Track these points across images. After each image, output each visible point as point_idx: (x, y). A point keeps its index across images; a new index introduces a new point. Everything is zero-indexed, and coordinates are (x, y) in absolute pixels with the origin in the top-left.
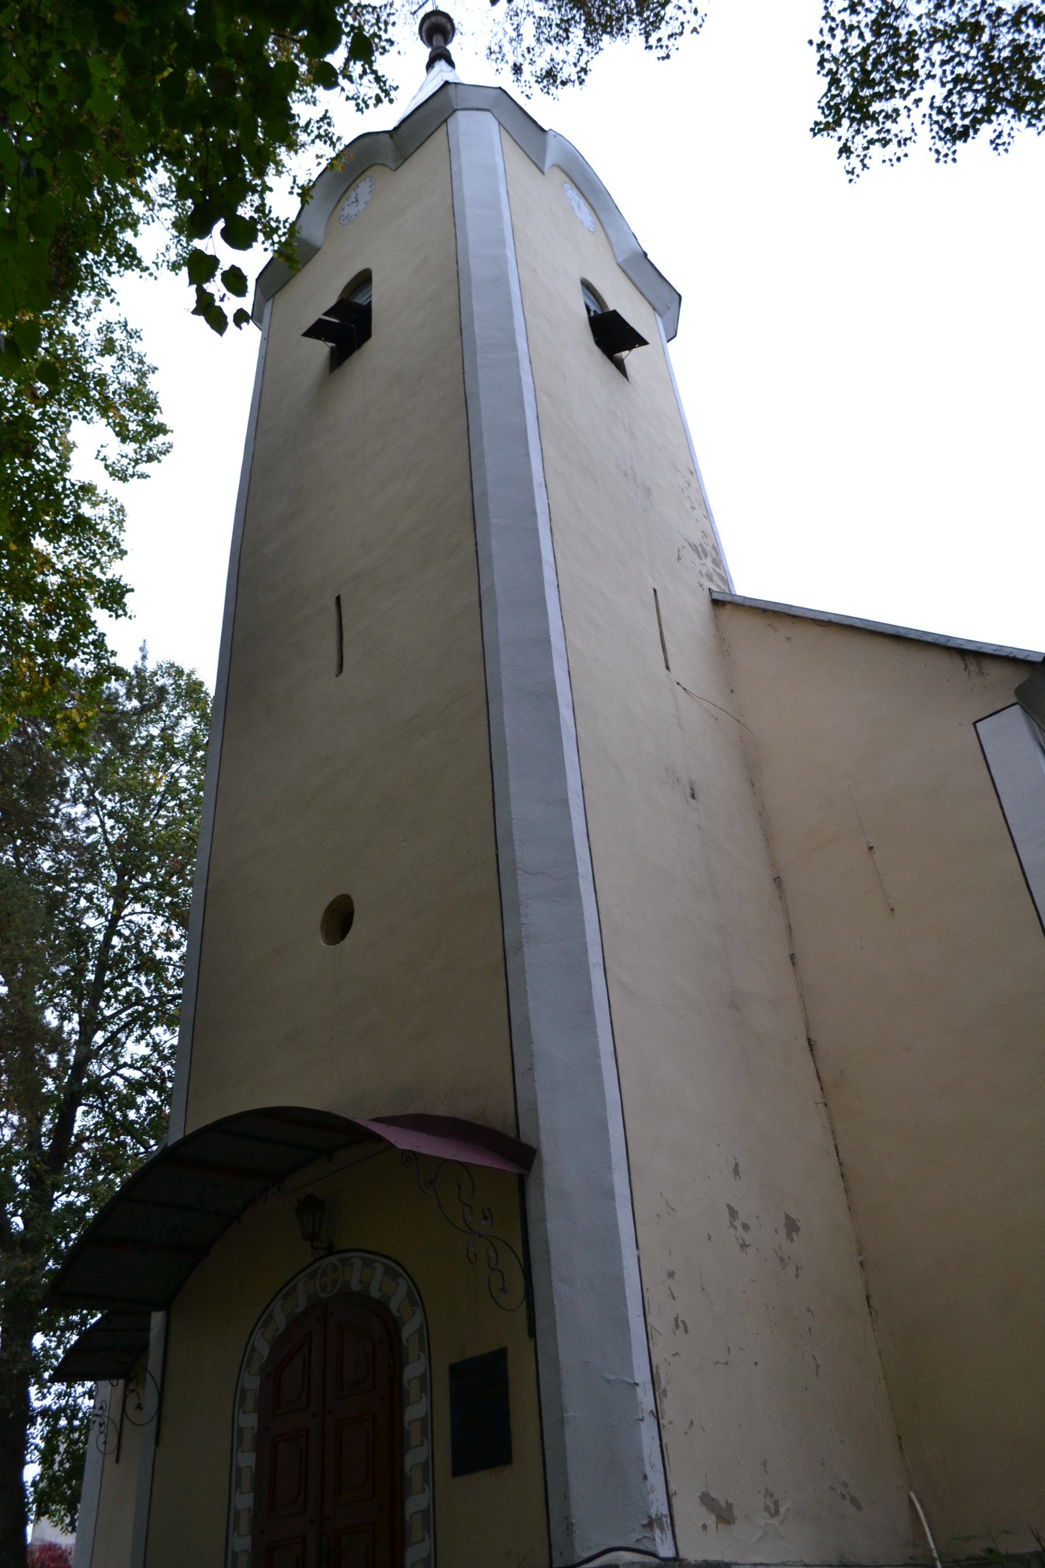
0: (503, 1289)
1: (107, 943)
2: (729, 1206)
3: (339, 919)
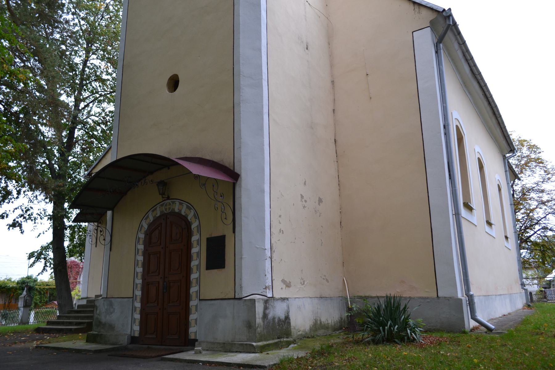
0: (226, 218)
1: (83, 70)
2: (301, 195)
3: (174, 83)
